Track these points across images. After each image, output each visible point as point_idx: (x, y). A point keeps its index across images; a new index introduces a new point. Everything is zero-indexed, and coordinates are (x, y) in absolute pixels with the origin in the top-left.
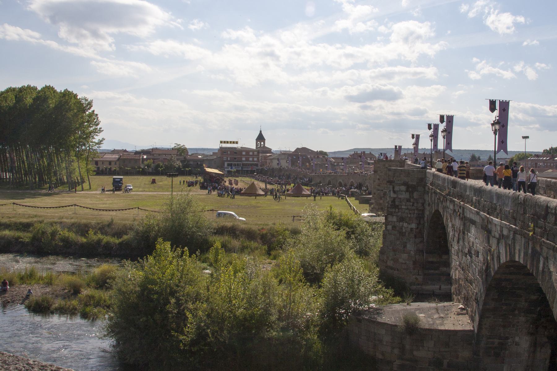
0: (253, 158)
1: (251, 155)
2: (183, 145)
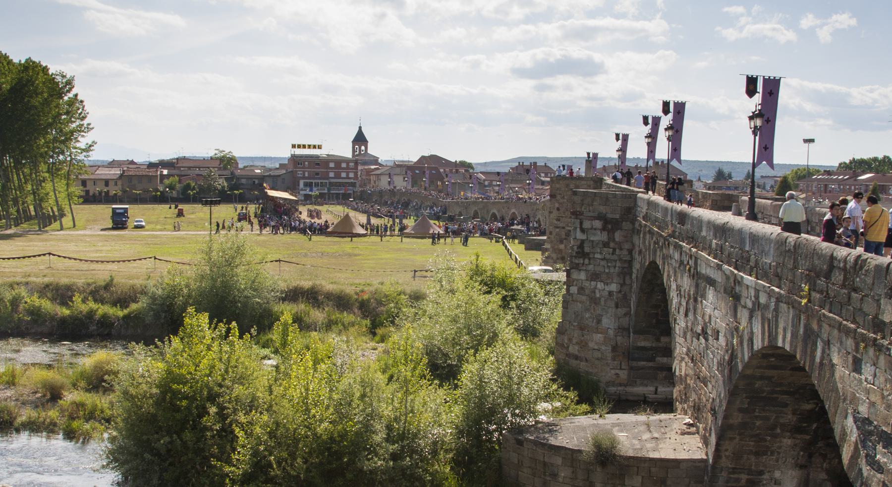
0: (348, 174)
1: (344, 168)
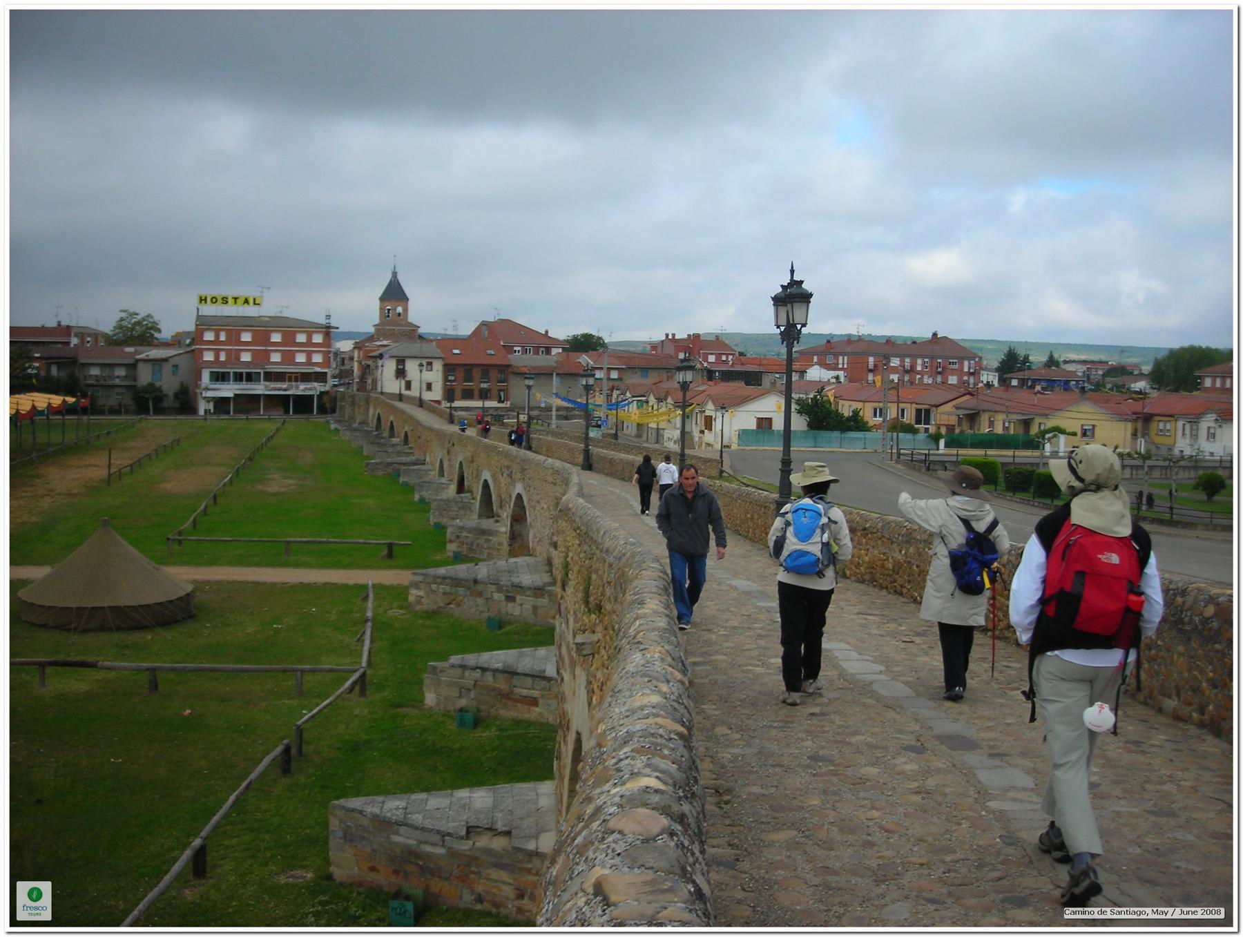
0: (217, 352)
1: (301, 344)
2: (146, 314)
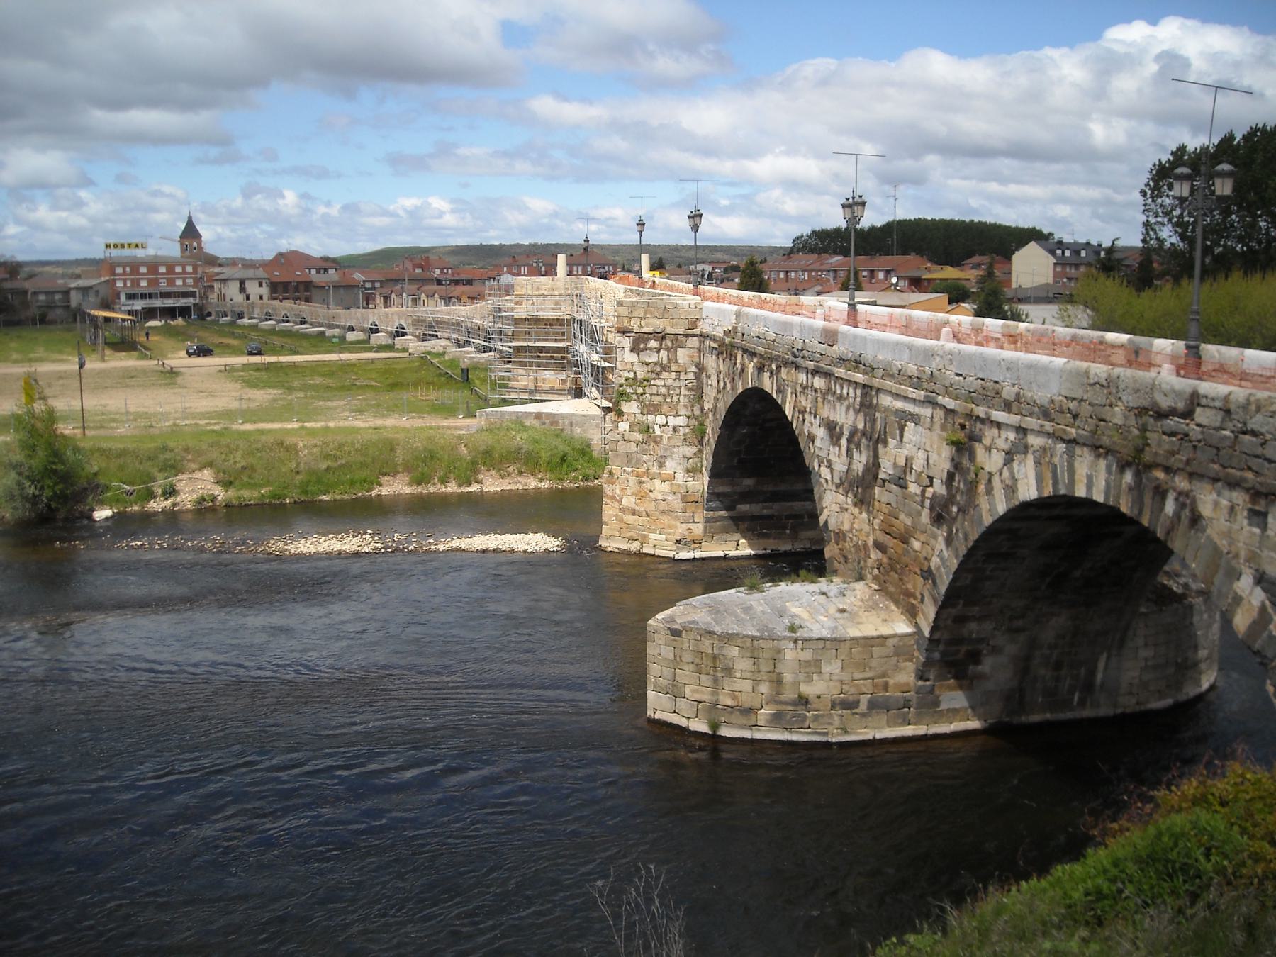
0: (184, 280)
1: (179, 273)
